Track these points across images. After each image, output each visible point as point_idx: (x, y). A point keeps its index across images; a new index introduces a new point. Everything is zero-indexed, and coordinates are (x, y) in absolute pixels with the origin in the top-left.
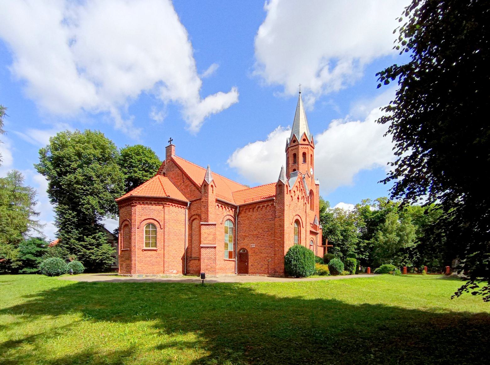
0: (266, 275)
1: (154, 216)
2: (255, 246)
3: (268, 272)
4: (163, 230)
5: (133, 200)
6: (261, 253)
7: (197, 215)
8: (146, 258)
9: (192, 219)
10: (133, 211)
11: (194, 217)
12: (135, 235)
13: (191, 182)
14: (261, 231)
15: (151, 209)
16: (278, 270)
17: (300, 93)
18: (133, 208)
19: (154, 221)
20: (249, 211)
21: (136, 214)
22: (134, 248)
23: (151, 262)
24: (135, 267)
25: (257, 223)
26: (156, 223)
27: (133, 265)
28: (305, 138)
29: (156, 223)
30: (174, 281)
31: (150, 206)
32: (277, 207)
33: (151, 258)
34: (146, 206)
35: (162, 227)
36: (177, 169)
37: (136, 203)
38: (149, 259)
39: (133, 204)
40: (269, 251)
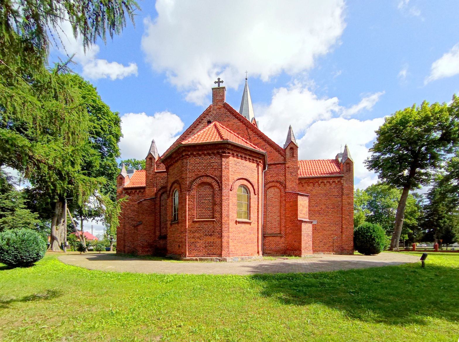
0: (332, 253)
1: (247, 176)
2: (316, 223)
3: (333, 250)
4: (257, 196)
5: (225, 148)
6: (325, 230)
7: (277, 182)
8: (239, 233)
9: (268, 186)
10: (223, 163)
11: (271, 184)
12: (228, 199)
13: (263, 139)
14: (324, 207)
15: (244, 165)
16: (346, 247)
17: (246, 79)
18: (223, 159)
19: (249, 184)
20: (308, 185)
21: (228, 169)
22: (226, 219)
23: (245, 239)
24: (228, 247)
25: (319, 199)
26: (249, 186)
27: (224, 244)
28: (255, 123)
29: (249, 186)
30: (386, 263)
31: (243, 161)
32: (345, 185)
33: (245, 234)
34: (239, 160)
35: (256, 193)
36: (236, 120)
37: (229, 153)
38: (242, 235)
39: (226, 153)
40: (334, 228)
